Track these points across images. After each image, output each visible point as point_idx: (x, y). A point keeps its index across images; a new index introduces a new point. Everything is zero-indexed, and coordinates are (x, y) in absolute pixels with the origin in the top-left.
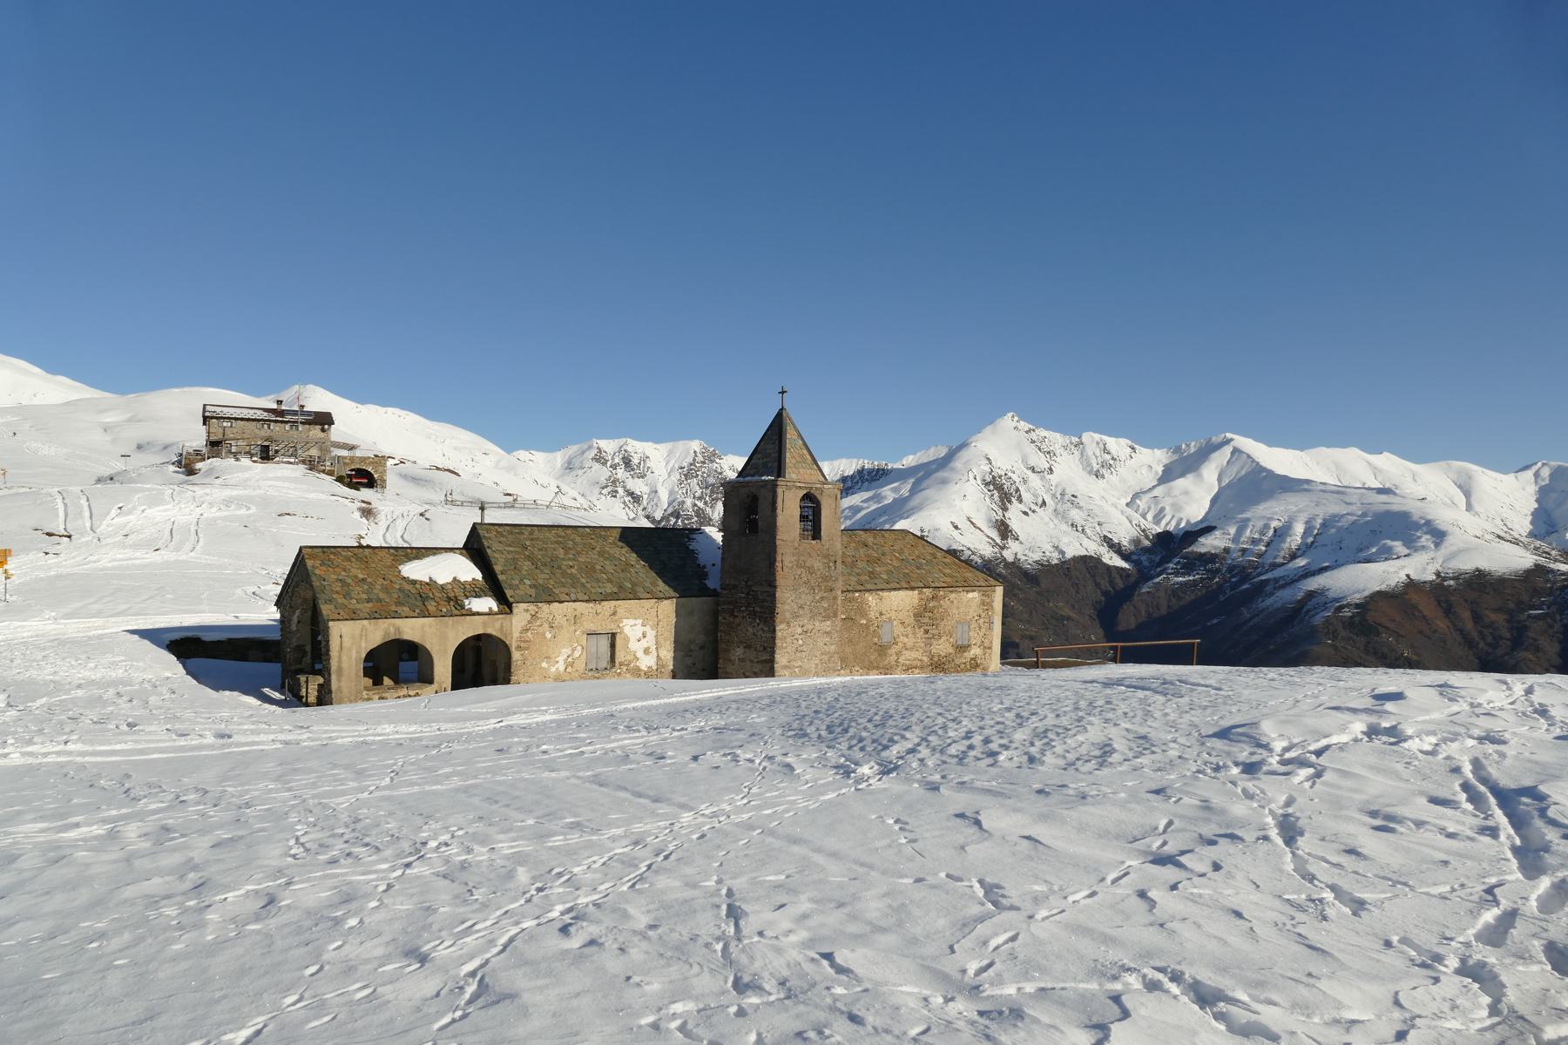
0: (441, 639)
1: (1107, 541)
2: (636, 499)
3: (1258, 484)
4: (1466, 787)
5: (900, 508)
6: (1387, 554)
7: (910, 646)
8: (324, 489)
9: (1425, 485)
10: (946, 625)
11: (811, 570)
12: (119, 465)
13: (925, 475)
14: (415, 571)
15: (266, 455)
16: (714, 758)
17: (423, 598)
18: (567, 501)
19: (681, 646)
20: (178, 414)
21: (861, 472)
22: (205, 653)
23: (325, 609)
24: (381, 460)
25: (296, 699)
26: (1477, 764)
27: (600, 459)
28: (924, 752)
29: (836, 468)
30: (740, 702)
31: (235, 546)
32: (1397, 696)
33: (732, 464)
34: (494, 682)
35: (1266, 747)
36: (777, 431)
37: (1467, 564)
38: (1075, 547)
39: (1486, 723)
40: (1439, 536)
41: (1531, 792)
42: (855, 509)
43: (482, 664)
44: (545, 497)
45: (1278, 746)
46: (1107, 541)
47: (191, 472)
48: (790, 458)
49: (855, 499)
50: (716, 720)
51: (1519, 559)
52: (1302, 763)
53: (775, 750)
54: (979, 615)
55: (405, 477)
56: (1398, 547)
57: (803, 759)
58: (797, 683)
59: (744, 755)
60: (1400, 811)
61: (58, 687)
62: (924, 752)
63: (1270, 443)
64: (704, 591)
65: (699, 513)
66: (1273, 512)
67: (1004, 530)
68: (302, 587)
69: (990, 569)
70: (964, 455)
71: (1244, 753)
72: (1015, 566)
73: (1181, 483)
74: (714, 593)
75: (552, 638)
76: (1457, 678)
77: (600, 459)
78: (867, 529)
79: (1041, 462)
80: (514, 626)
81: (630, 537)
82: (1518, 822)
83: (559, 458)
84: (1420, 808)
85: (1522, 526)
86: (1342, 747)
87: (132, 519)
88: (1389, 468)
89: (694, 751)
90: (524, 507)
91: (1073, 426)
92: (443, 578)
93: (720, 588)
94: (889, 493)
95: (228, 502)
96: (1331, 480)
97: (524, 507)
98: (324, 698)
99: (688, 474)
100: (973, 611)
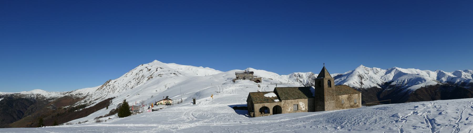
0: (271, 106)
1: (378, 84)
2: (301, 82)
3: (400, 74)
4: (426, 120)
5: (345, 81)
6: (418, 84)
7: (347, 104)
8: (253, 83)
9: (423, 73)
10: (353, 100)
11: (330, 93)
12: (225, 82)
13: (349, 75)
14: (266, 95)
15: (244, 79)
16: (314, 127)
17: (268, 100)
18: (290, 83)
19: (309, 106)
20: (232, 74)
21: (338, 75)
22: (238, 109)
23: (254, 102)
24: (261, 78)
25: (250, 116)
26: (427, 116)
27: (295, 76)
28: (348, 124)
29: (333, 75)
30: (318, 116)
31: (240, 92)
32: (417, 107)
33: (316, 75)
34: (279, 113)
35: (399, 117)
36: (323, 70)
37: (429, 84)
38: (373, 85)
39: (429, 109)
40: (425, 80)
41: (434, 119)
42: (337, 81)
43: (277, 110)
44: (286, 82)
45: (401, 117)
46: (378, 84)
47: (234, 82)
48: (325, 75)
49: (337, 80)
50: (314, 120)
51: (436, 83)
52: (404, 119)
53: (324, 125)
54: (358, 98)
55: (264, 80)
56: (420, 82)
57: (329, 126)
58: (328, 112)
59: (319, 126)
60: (418, 125)
61: (219, 114)
62: (348, 124)
63: (406, 68)
64: (312, 97)
65: (311, 83)
66: (403, 78)
67: (362, 83)
68: (251, 98)
69: (359, 90)
70: (355, 72)
71: (396, 119)
72: (364, 89)
73: (388, 75)
74: (314, 97)
75: (288, 106)
76: (425, 103)
77: (295, 76)
78: (340, 84)
79: (367, 72)
80: (282, 104)
81: (300, 88)
82: (432, 124)
83: (288, 76)
84: (420, 124)
85: (436, 79)
86: (410, 116)
87: (227, 89)
88: (418, 71)
89: (311, 125)
90: (283, 84)
91: (371, 67)
92: (271, 97)
93: (315, 96)
94: (343, 79)
95: (239, 86)
96: (411, 73)
97: (283, 84)
98: (254, 116)
99: (309, 77)
100: (357, 97)
